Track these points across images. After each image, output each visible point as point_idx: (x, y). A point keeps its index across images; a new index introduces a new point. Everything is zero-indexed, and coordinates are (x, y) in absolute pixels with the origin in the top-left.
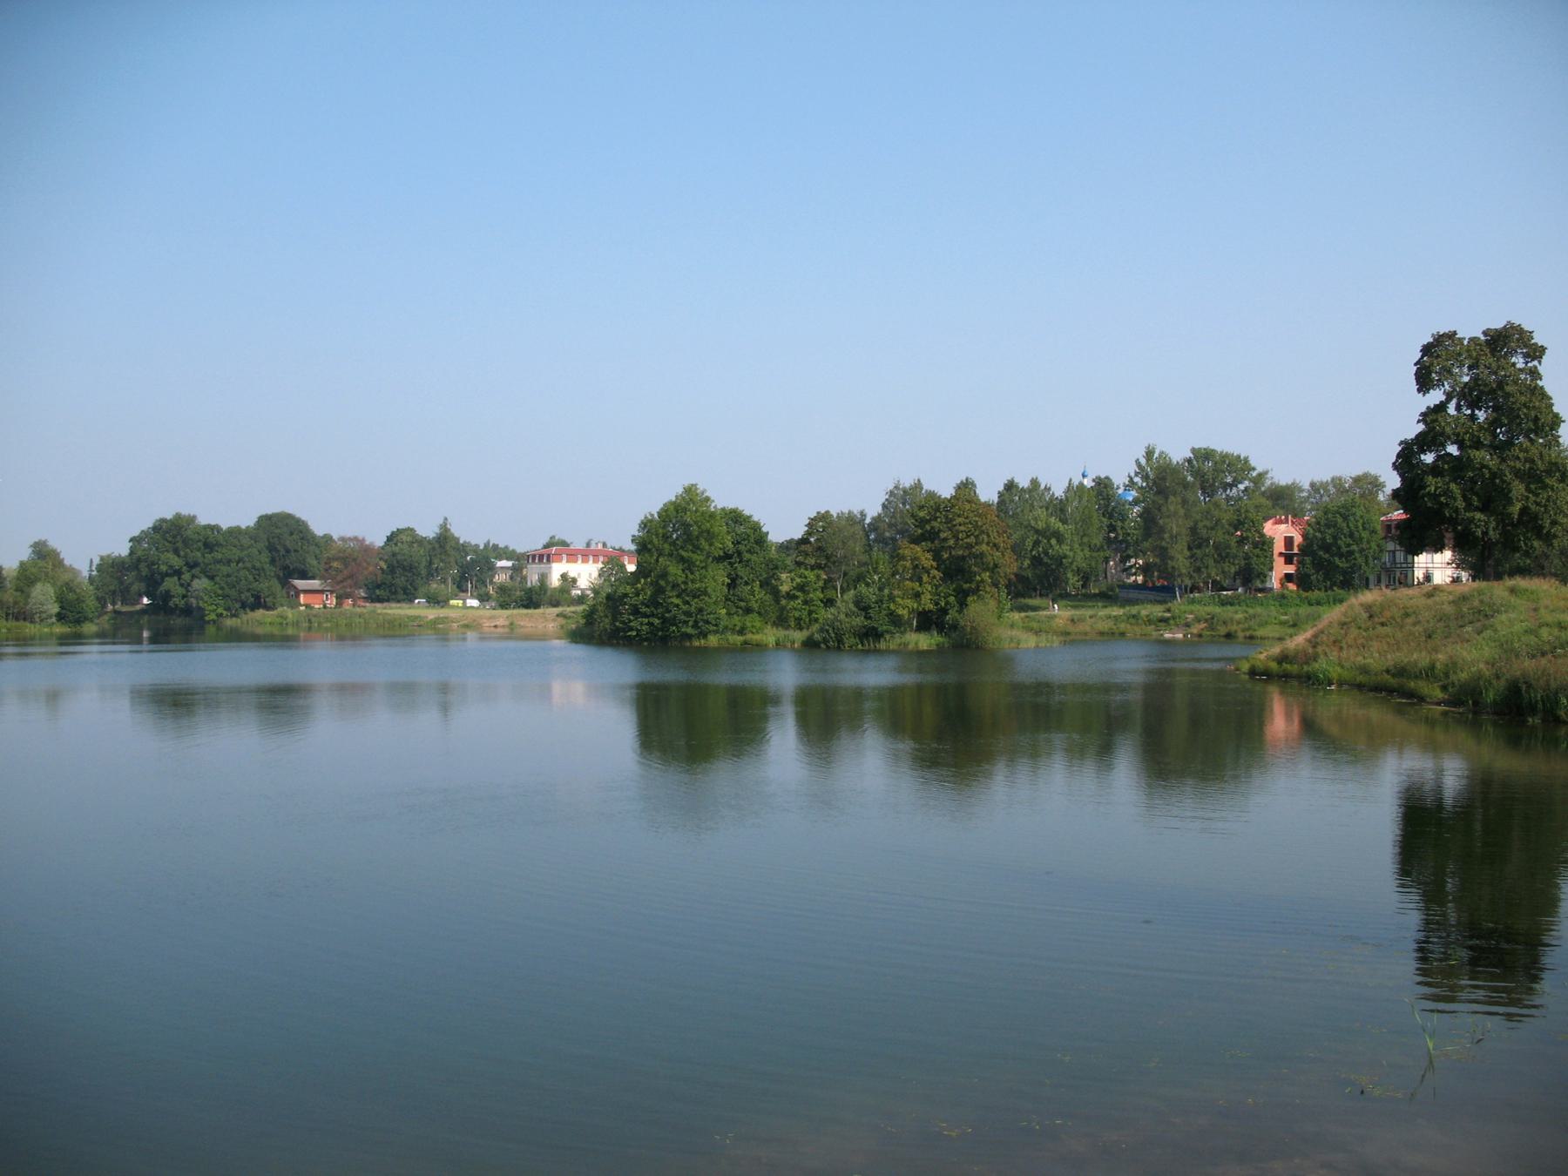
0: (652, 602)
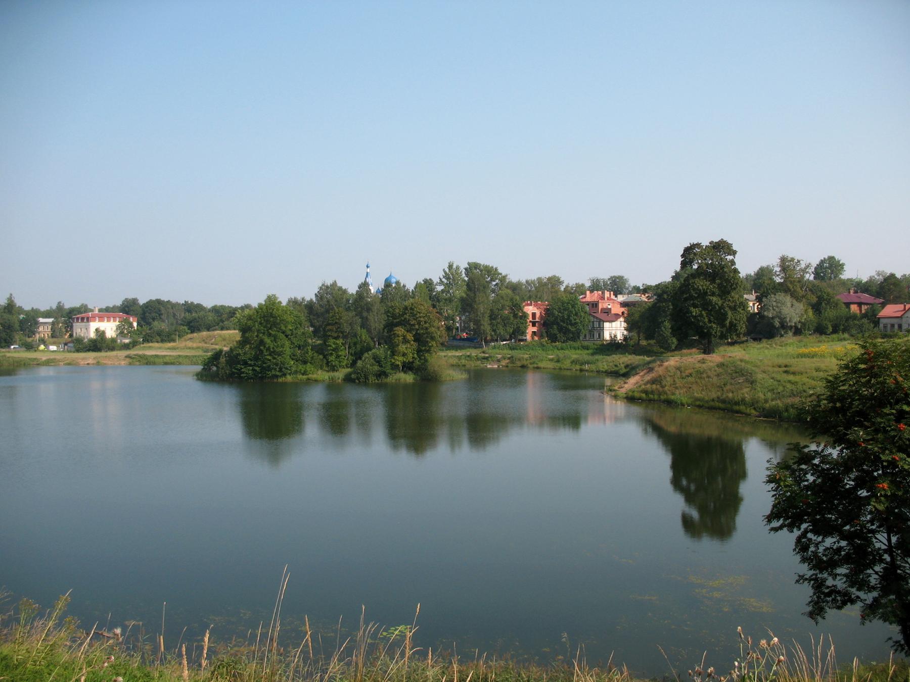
0: (256, 358)
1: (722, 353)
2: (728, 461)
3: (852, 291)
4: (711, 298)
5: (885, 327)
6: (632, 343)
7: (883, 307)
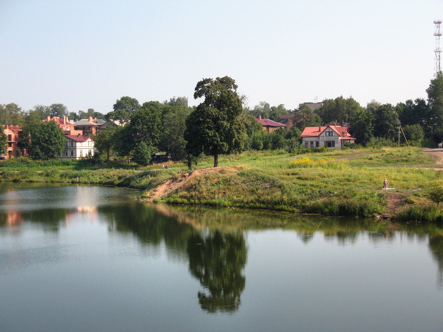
2: (236, 248)
4: (222, 122)
5: (306, 144)
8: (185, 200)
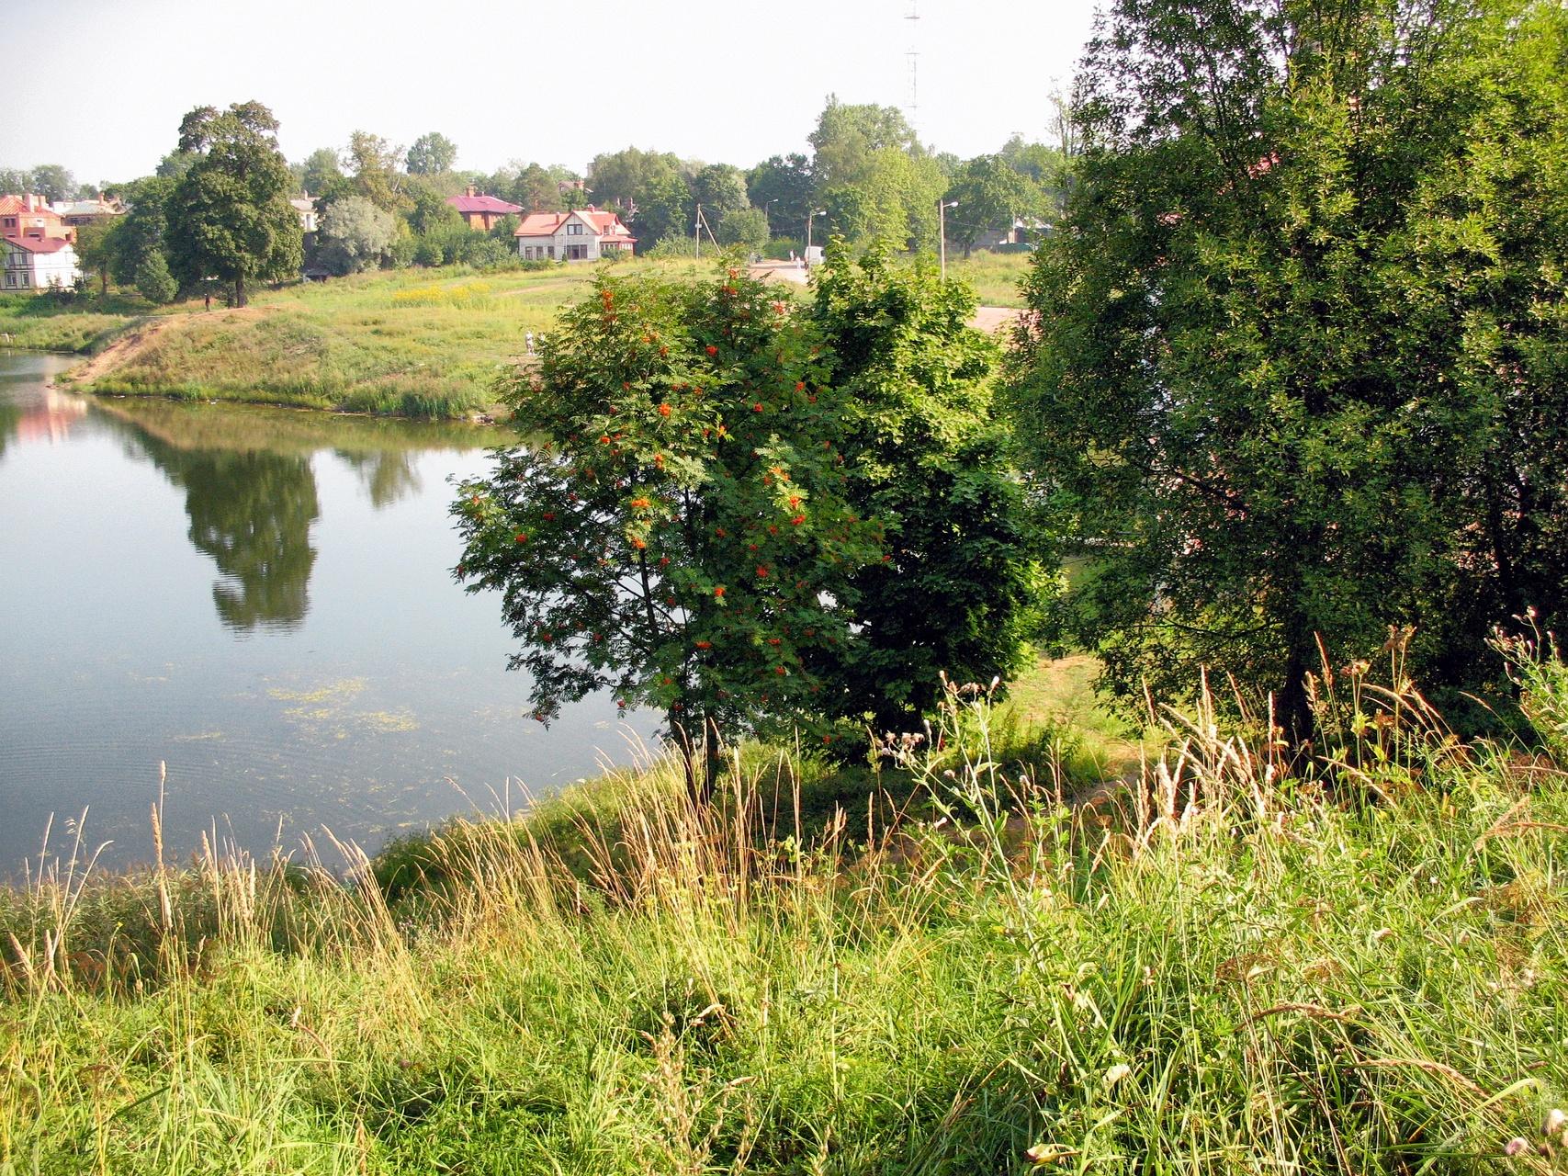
1: (262, 304)
3: (472, 193)
4: (238, 206)
6: (92, 291)
7: (523, 220)
8: (128, 386)
